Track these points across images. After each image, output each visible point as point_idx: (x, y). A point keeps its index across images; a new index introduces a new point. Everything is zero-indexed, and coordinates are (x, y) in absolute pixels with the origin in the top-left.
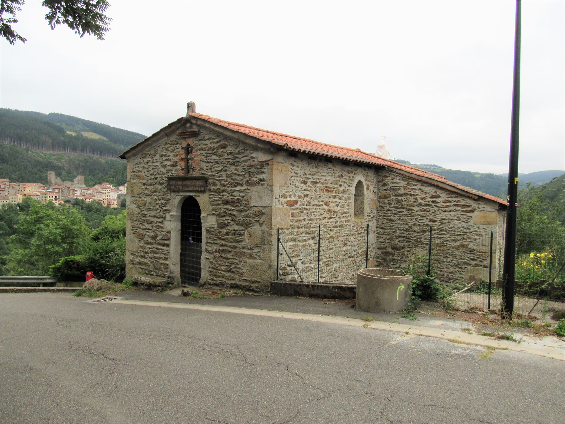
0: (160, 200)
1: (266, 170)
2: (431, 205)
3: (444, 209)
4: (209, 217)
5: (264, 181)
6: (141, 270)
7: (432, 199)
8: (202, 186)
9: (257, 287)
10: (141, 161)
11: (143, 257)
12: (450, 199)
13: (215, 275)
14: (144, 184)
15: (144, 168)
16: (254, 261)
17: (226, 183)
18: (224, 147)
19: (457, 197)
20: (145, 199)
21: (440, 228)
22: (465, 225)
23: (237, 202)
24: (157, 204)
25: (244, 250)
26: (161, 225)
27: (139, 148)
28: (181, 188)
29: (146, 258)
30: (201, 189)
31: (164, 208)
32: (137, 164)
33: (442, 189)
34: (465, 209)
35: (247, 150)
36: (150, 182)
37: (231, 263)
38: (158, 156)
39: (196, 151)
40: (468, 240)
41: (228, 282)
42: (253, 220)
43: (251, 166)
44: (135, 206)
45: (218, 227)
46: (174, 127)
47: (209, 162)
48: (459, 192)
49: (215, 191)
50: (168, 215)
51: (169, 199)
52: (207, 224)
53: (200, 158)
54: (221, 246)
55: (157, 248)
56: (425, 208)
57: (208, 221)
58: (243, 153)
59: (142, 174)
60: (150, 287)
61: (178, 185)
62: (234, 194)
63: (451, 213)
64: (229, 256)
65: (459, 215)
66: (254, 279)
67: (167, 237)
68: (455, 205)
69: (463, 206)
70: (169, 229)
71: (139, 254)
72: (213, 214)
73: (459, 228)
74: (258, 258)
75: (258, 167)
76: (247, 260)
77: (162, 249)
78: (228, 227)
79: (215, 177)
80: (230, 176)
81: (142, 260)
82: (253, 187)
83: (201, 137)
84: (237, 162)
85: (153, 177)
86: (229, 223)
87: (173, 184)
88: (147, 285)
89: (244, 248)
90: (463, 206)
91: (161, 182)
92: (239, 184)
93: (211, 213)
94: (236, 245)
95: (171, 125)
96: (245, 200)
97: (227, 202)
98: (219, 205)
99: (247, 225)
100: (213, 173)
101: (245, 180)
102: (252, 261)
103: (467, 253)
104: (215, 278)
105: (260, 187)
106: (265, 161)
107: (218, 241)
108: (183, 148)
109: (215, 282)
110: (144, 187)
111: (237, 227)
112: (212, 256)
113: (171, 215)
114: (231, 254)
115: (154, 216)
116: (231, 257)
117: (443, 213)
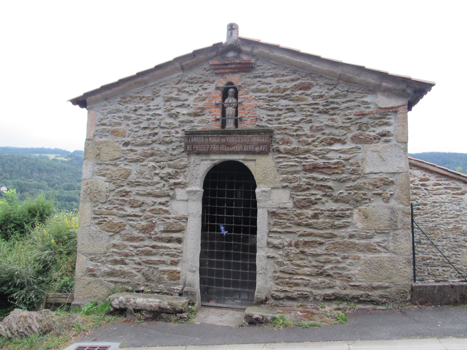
0: (163, 168)
1: (392, 121)
2: (421, 188)
3: (434, 192)
4: (274, 191)
5: (389, 136)
6: (113, 285)
7: (421, 183)
8: (264, 144)
9: (382, 296)
10: (121, 107)
11: (123, 262)
12: (440, 182)
13: (287, 283)
14: (126, 144)
15: (127, 118)
16: (376, 255)
17: (310, 140)
18: (308, 87)
19: (447, 180)
20: (127, 167)
21: (431, 212)
22: (458, 208)
23: (335, 168)
24: (156, 174)
25: (351, 240)
26: (164, 208)
27: (120, 87)
28: (215, 148)
29: (126, 264)
30: (262, 148)
31: (172, 181)
32: (110, 113)
33: (431, 172)
34: (456, 192)
35: (353, 92)
36: (139, 140)
37: (325, 262)
38: (159, 101)
39: (247, 93)
40: (461, 222)
41: (315, 292)
42: (370, 194)
43: (363, 115)
44: (104, 178)
45: (294, 207)
46: (202, 57)
47: (273, 110)
48: (454, 176)
49: (288, 152)
50: (180, 193)
51: (185, 167)
52: (270, 202)
53: (254, 103)
54: (301, 235)
55: (153, 247)
56: (415, 191)
57: (271, 196)
58: (345, 96)
59: (123, 127)
60: (157, 314)
61: (210, 144)
62: (330, 155)
63: (441, 196)
64: (319, 250)
65: (450, 198)
66: (375, 284)
67: (178, 228)
68: (445, 188)
69: (453, 189)
70: (182, 213)
71: (110, 259)
72: (284, 187)
73: (451, 210)
74: (382, 250)
75: (378, 116)
76: (361, 255)
77: (165, 248)
78: (316, 206)
79: (287, 131)
80: (319, 129)
81: (117, 267)
82: (366, 145)
83: (258, 72)
84: (333, 109)
85: (148, 132)
86: (320, 199)
87: (194, 143)
88: (150, 312)
89: (351, 236)
90: (453, 189)
91: (167, 139)
92: (339, 141)
93: (279, 185)
94: (335, 232)
95: (196, 53)
96: (352, 165)
97: (315, 168)
98: (296, 172)
99: (357, 201)
100: (284, 126)
101: (350, 135)
102: (370, 256)
103: (461, 235)
104: (287, 289)
105: (380, 146)
106: (392, 108)
107: (294, 229)
108: (217, 88)
109: (290, 295)
110: (125, 148)
111: (334, 206)
112: (281, 252)
113: (189, 192)
114: (324, 247)
115: (149, 194)
116: (326, 252)
117: (433, 196)
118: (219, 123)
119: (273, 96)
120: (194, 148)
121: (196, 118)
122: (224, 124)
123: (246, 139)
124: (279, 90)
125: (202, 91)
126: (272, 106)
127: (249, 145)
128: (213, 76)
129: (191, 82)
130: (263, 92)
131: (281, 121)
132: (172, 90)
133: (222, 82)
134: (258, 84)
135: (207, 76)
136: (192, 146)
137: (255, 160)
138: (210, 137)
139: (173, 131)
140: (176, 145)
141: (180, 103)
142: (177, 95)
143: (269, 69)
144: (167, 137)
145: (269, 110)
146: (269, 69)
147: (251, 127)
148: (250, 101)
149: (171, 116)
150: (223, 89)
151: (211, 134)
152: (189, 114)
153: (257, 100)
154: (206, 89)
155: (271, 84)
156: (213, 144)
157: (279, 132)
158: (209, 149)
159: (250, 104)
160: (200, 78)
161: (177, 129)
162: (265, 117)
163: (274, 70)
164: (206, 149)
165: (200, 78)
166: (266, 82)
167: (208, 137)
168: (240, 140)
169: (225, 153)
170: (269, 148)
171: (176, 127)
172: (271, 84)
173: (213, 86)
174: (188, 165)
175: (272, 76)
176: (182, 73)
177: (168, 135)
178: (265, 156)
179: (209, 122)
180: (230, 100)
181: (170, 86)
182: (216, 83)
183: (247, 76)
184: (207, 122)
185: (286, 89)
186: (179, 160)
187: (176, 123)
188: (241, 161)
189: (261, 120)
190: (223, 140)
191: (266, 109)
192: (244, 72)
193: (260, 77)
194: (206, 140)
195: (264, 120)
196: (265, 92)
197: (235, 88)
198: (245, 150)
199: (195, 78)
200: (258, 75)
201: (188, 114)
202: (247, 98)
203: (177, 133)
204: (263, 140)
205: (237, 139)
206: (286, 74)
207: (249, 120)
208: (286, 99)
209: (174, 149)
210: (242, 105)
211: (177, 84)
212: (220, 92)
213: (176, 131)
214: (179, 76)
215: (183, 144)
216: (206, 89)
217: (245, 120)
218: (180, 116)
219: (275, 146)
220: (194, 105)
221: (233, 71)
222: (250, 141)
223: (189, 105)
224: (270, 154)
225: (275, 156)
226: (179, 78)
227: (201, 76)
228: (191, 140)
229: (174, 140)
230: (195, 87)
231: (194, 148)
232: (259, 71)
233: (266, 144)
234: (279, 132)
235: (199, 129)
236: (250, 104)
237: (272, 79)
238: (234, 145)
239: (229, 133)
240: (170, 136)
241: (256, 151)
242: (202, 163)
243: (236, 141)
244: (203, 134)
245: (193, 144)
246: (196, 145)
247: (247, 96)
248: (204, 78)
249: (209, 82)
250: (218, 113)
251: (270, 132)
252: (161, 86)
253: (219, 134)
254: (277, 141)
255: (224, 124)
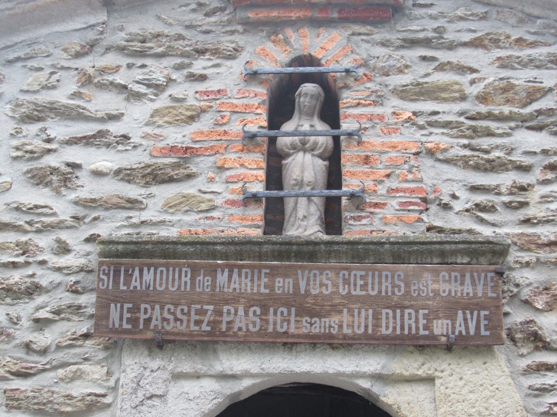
8: (471, 305)
28: (243, 320)
30: (465, 324)
39: (379, 101)
47: (492, 167)
53: (410, 137)
61: (220, 300)
91: (16, 277)
108: (253, 76)
118: (257, 213)
119: (489, 116)
120: (143, 317)
121: (154, 189)
122: (275, 214)
123: (388, 279)
124: (510, 95)
125: (187, 85)
126: (487, 152)
127: (403, 308)
128: (233, 32)
129: (138, 50)
130: (445, 100)
131: (534, 211)
132: (55, 77)
133: (272, 57)
134: (423, 68)
135: (207, 32)
136: (135, 309)
137: (430, 380)
138: (223, 267)
139: (44, 241)
140: (54, 305)
141: (90, 129)
142: (76, 95)
143: (461, 19)
144: (14, 265)
145: (477, 168)
146: (461, 19)
147: (399, 231)
148: (392, 130)
149: (39, 178)
150: (274, 81)
151: (225, 256)
152: (125, 175)
153: (422, 128)
154: (203, 78)
155: (473, 71)
156: (233, 300)
157: (526, 257)
158: (214, 324)
159: (395, 139)
160: (180, 37)
161: (64, 235)
162: (463, 194)
163: (483, 24)
164: (198, 323)
165: (180, 37)
166: (454, 60)
167: (212, 271)
168: (364, 287)
169: (289, 344)
170: (494, 325)
171: (59, 226)
172: (473, 71)
173: (237, 67)
174: (108, 400)
175: (476, 44)
176: (102, 17)
177: (21, 259)
178: (478, 363)
179: (213, 208)
180: (303, 124)
181: (48, 62)
182: (245, 56)
183: (377, 37)
184: (204, 206)
185: (539, 90)
186: (61, 372)
187: (63, 207)
188: (365, 384)
189: (446, 207)
190: (283, 285)
191: (464, 163)
192: (364, 22)
193: (426, 43)
194: (204, 282)
195: (458, 206)
196: (454, 100)
197: (320, 79)
198: (384, 331)
199: (158, 36)
200: (421, 35)
201: (118, 172)
202: (381, 118)
203: (63, 249)
204: (468, 289)
205: (346, 282)
206: (530, 38)
207: (394, 203)
208: (539, 128)
209: (40, 324)
210: (360, 143)
211: (78, 55)
212: (260, 94)
213: (59, 241)
214: (92, 26)
215: (87, 300)
216: (203, 78)
217: (376, 205)
218: (84, 178)
219: (518, 316)
220: (146, 136)
221: (317, 14)
222: (407, 293)
223: (126, 137)
224: (501, 353)
225: (524, 363)
226: (91, 35)
227: (184, 33)
228: (127, 283)
229: (44, 283)
230: (158, 70)
231: (143, 317)
232: (424, 21)
233: (481, 307)
234: (526, 257)
235: (170, 233)
236: (395, 139)
237: (480, 52)
238: (336, 309)
239: (307, 251)
240: (27, 264)
241: (434, 337)
242: (175, 389)
243: (343, 291)
244: (185, 256)
245: (136, 299)
246: (153, 303)
247: (378, 110)
248: (197, 39)
249: (216, 52)
250: (252, 172)
251: (495, 251)
252: (10, 62)
253: (260, 257)
254: (526, 293)
255: (275, 214)
